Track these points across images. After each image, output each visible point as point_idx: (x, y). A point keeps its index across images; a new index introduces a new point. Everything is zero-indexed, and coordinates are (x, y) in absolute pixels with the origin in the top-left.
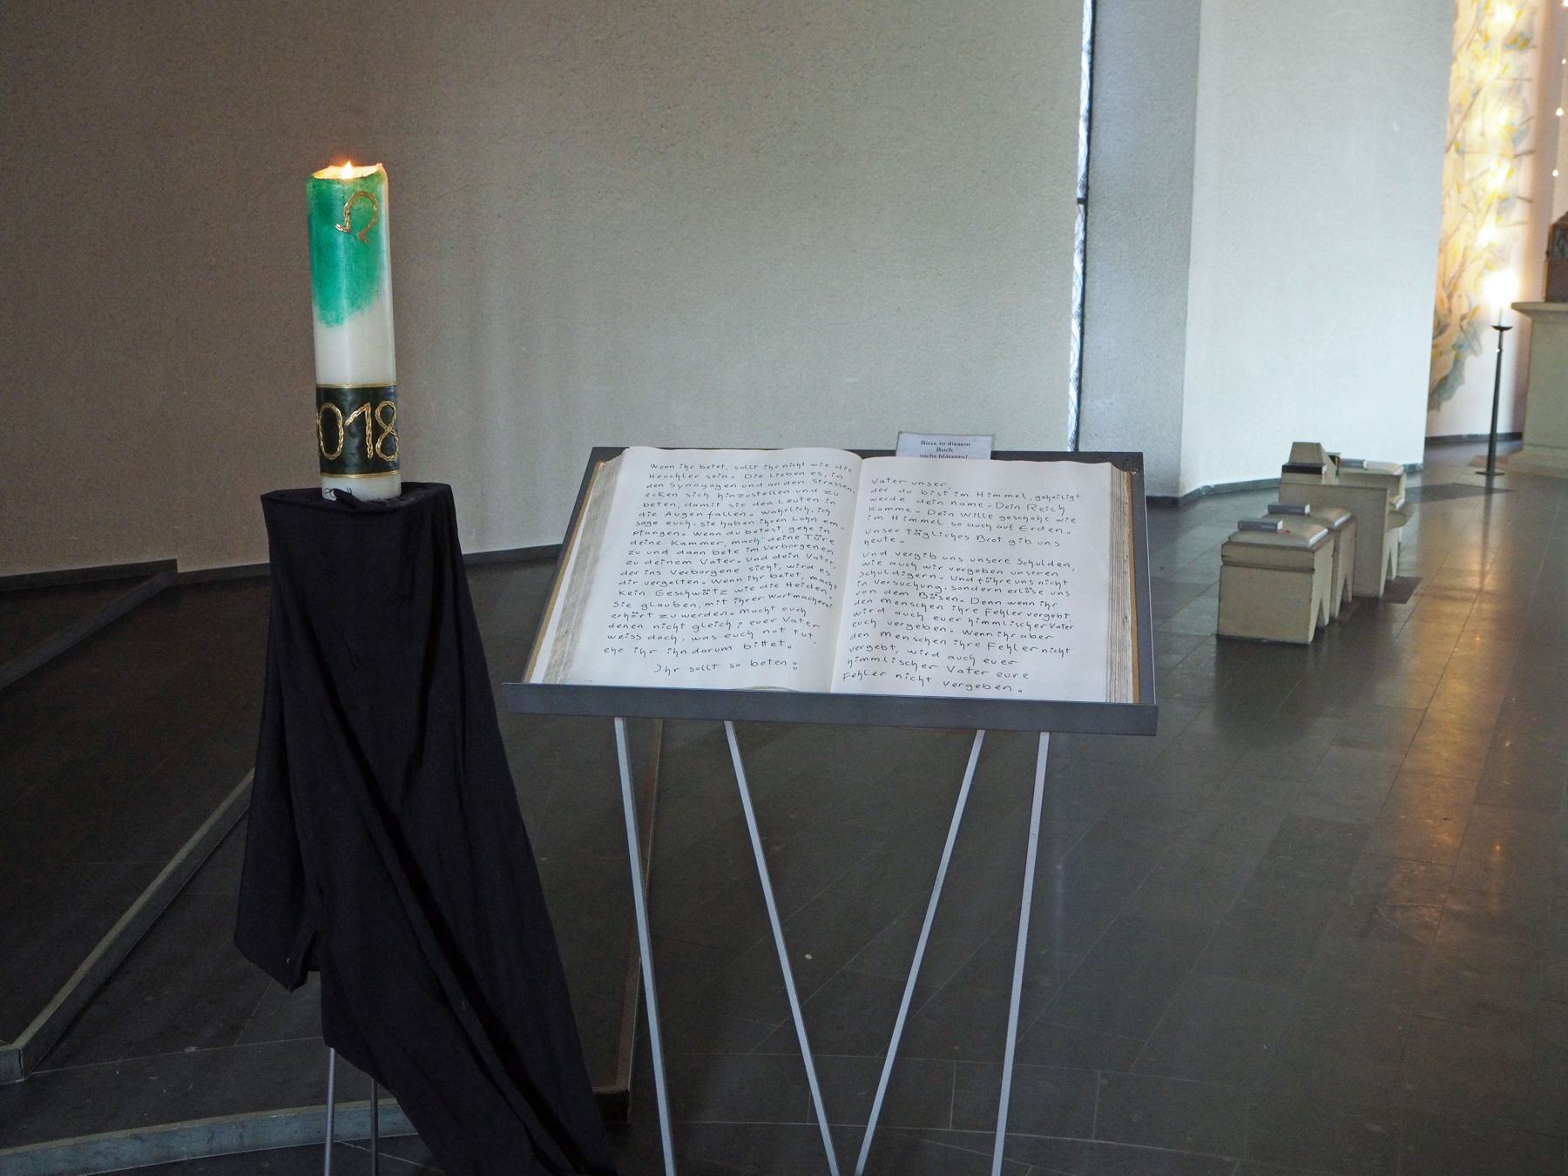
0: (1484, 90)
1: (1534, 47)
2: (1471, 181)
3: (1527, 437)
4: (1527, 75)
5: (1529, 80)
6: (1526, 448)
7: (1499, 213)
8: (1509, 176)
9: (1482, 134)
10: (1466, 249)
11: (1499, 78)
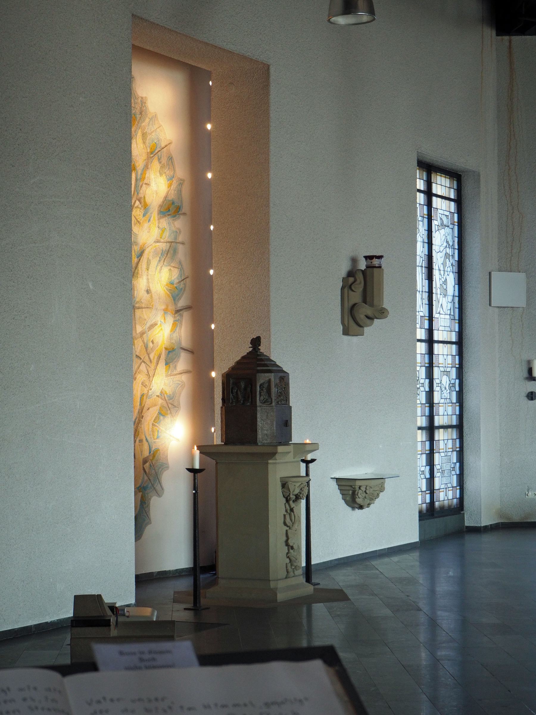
0: (146, 252)
1: (184, 214)
2: (142, 334)
3: (221, 570)
4: (180, 239)
5: (183, 243)
6: (221, 582)
7: (167, 364)
8: (173, 330)
9: (148, 291)
10: (142, 395)
11: (157, 241)
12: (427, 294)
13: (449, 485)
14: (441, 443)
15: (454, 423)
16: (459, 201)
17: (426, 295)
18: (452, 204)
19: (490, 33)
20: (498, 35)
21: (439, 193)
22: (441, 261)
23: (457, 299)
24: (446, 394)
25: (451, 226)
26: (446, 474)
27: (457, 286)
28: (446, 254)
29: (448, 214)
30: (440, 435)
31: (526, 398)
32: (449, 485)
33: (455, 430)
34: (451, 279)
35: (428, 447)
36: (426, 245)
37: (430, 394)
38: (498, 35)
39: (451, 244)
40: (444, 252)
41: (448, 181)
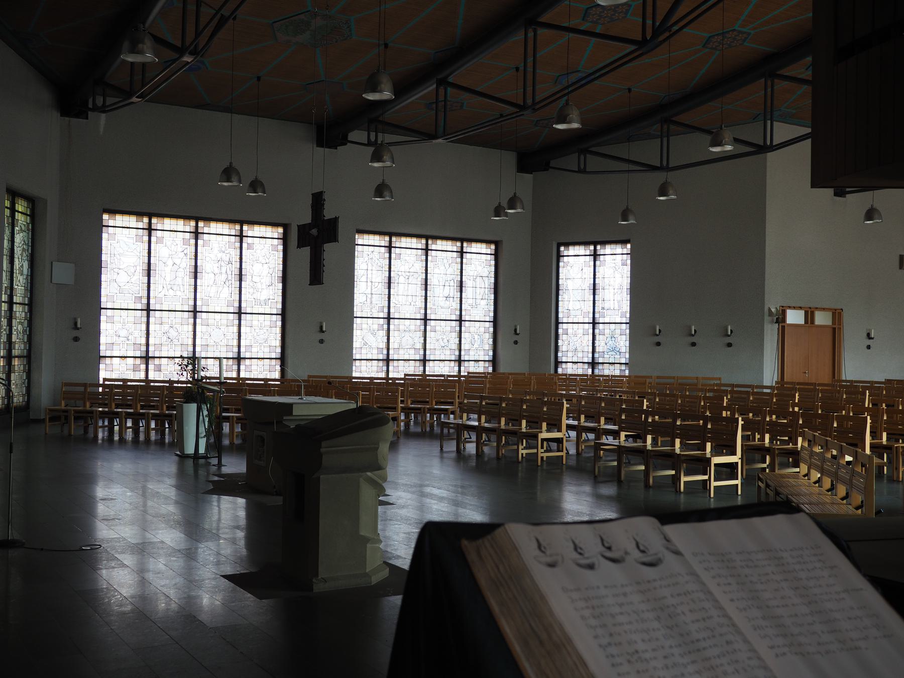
12: (10, 273)
13: (21, 393)
14: (16, 367)
15: (25, 355)
16: (33, 216)
17: (8, 274)
18: (28, 217)
19: (56, 115)
20: (61, 116)
21: (20, 210)
22: (20, 253)
23: (29, 277)
24: (20, 336)
25: (27, 232)
26: (19, 387)
27: (29, 269)
28: (23, 248)
29: (25, 223)
30: (16, 362)
31: (72, 341)
32: (21, 393)
33: (25, 359)
34: (26, 265)
35: (7, 369)
36: (10, 242)
37: (10, 336)
38: (61, 116)
39: (27, 242)
40: (22, 247)
41: (26, 203)
